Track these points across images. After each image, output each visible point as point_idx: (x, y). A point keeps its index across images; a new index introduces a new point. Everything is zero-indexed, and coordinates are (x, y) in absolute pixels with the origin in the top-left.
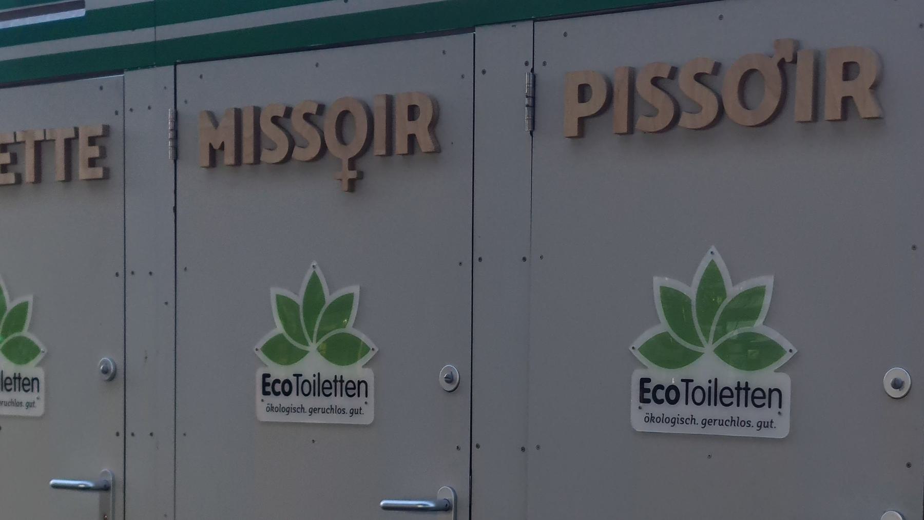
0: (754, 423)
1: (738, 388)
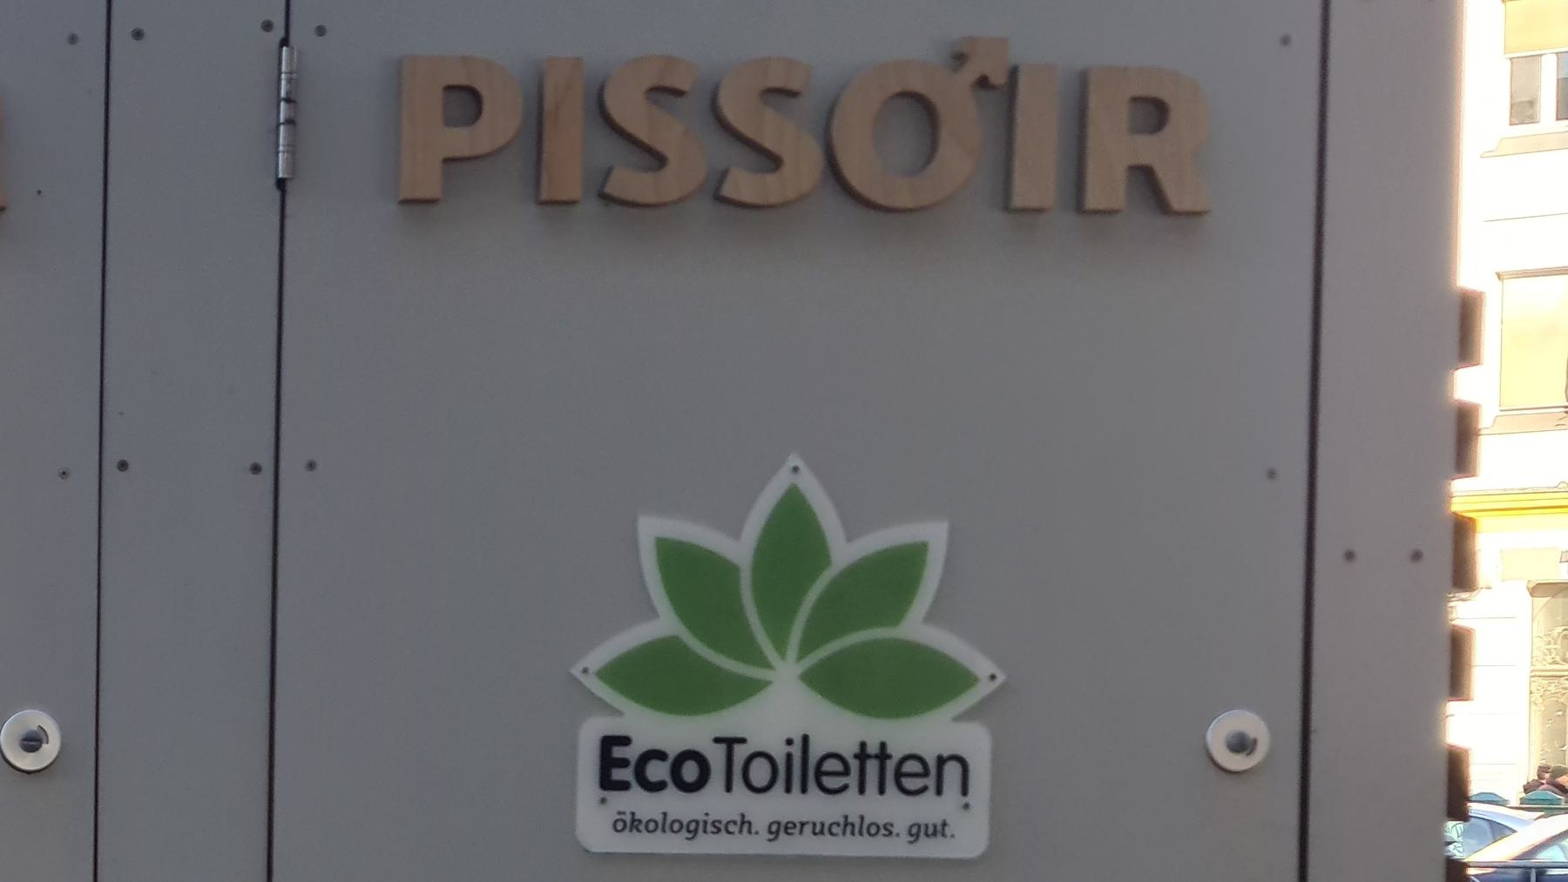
1: (862, 755)
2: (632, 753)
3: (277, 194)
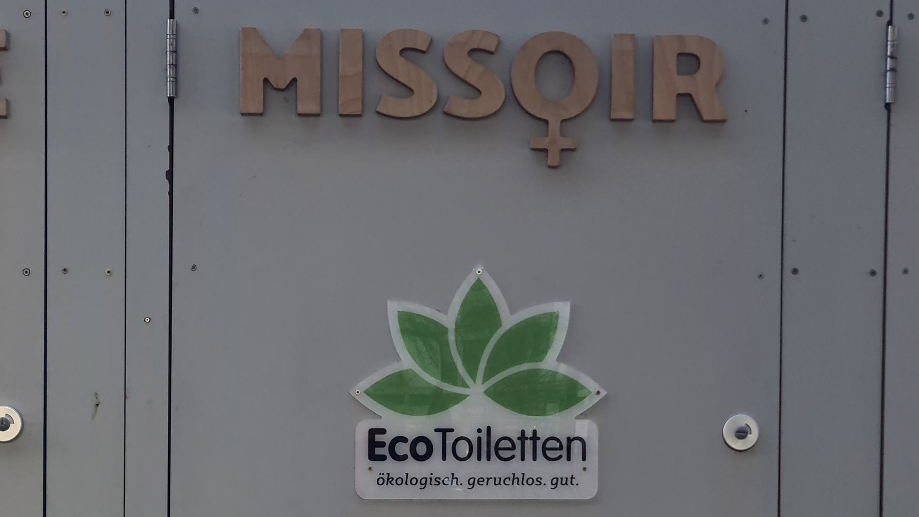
0: (547, 480)
1: (523, 438)
2: (387, 438)
3: (885, 112)
